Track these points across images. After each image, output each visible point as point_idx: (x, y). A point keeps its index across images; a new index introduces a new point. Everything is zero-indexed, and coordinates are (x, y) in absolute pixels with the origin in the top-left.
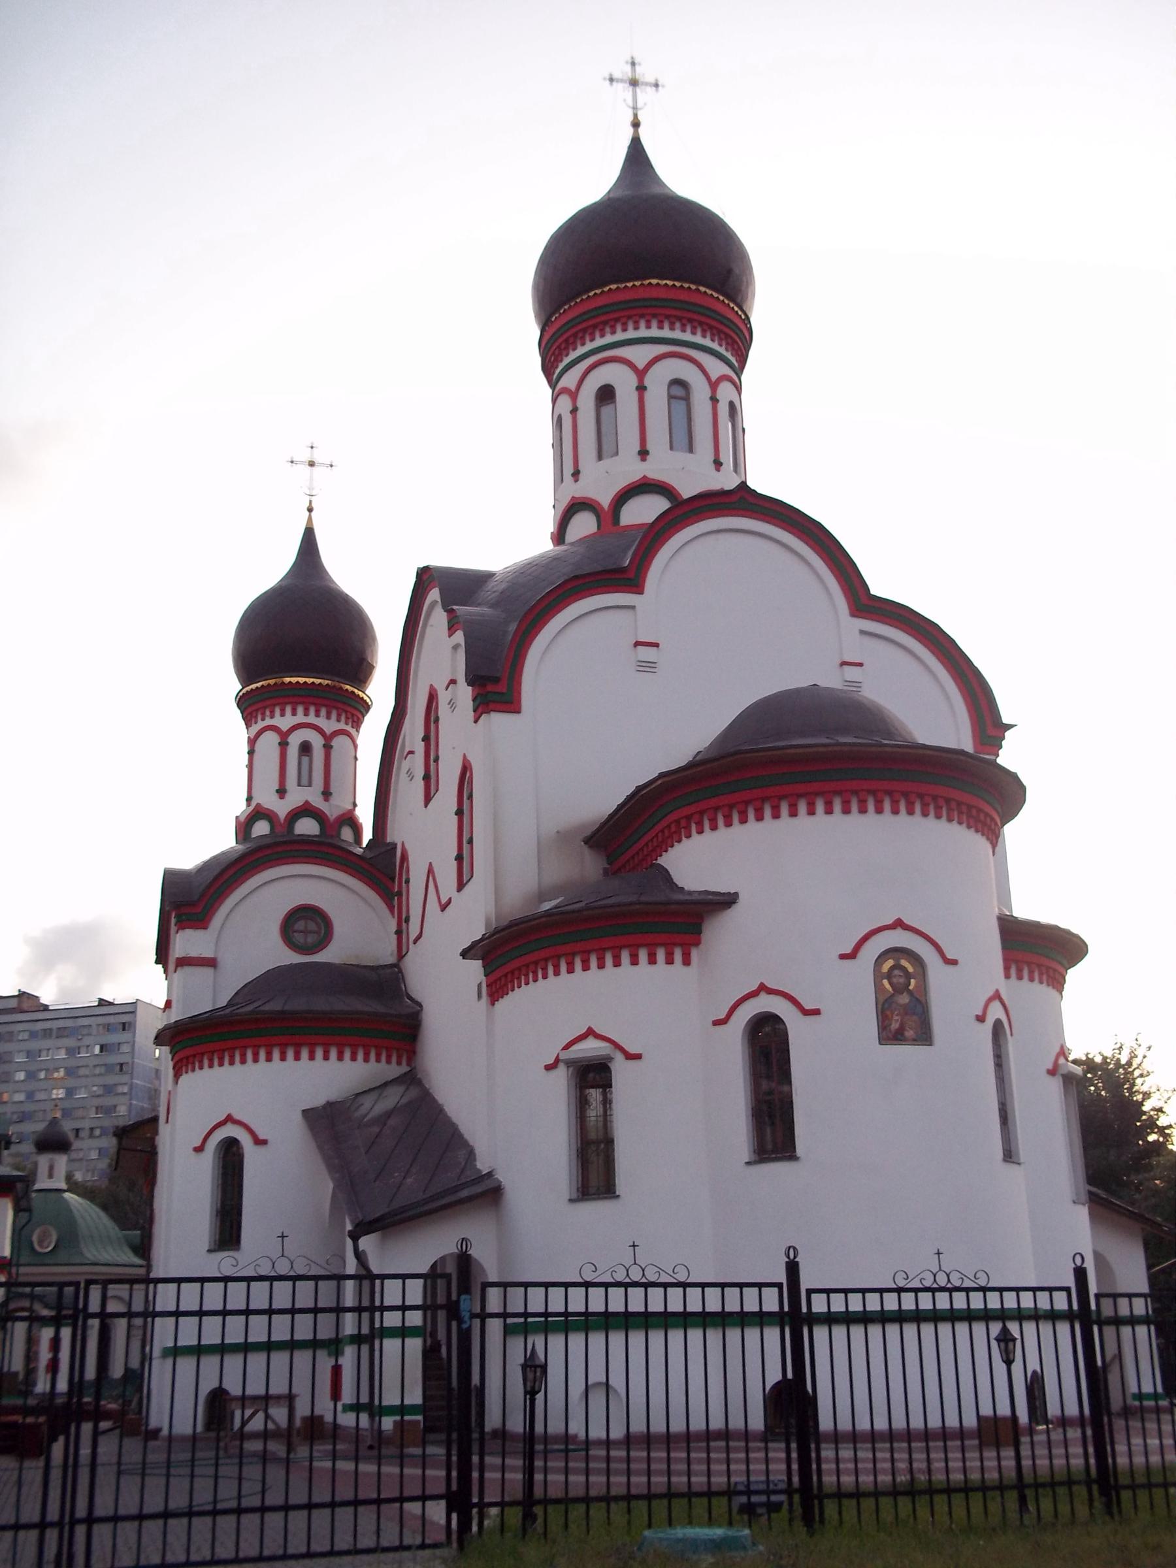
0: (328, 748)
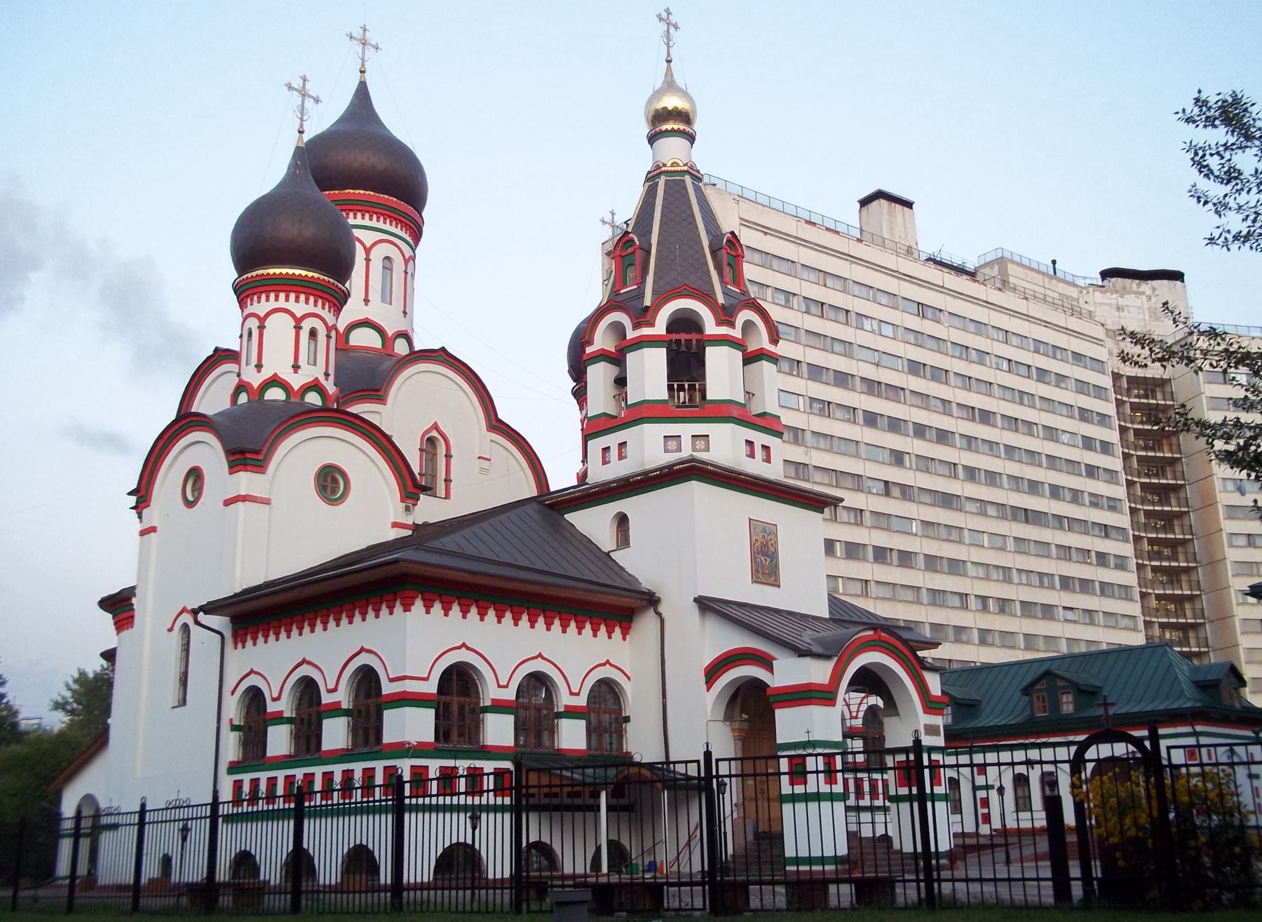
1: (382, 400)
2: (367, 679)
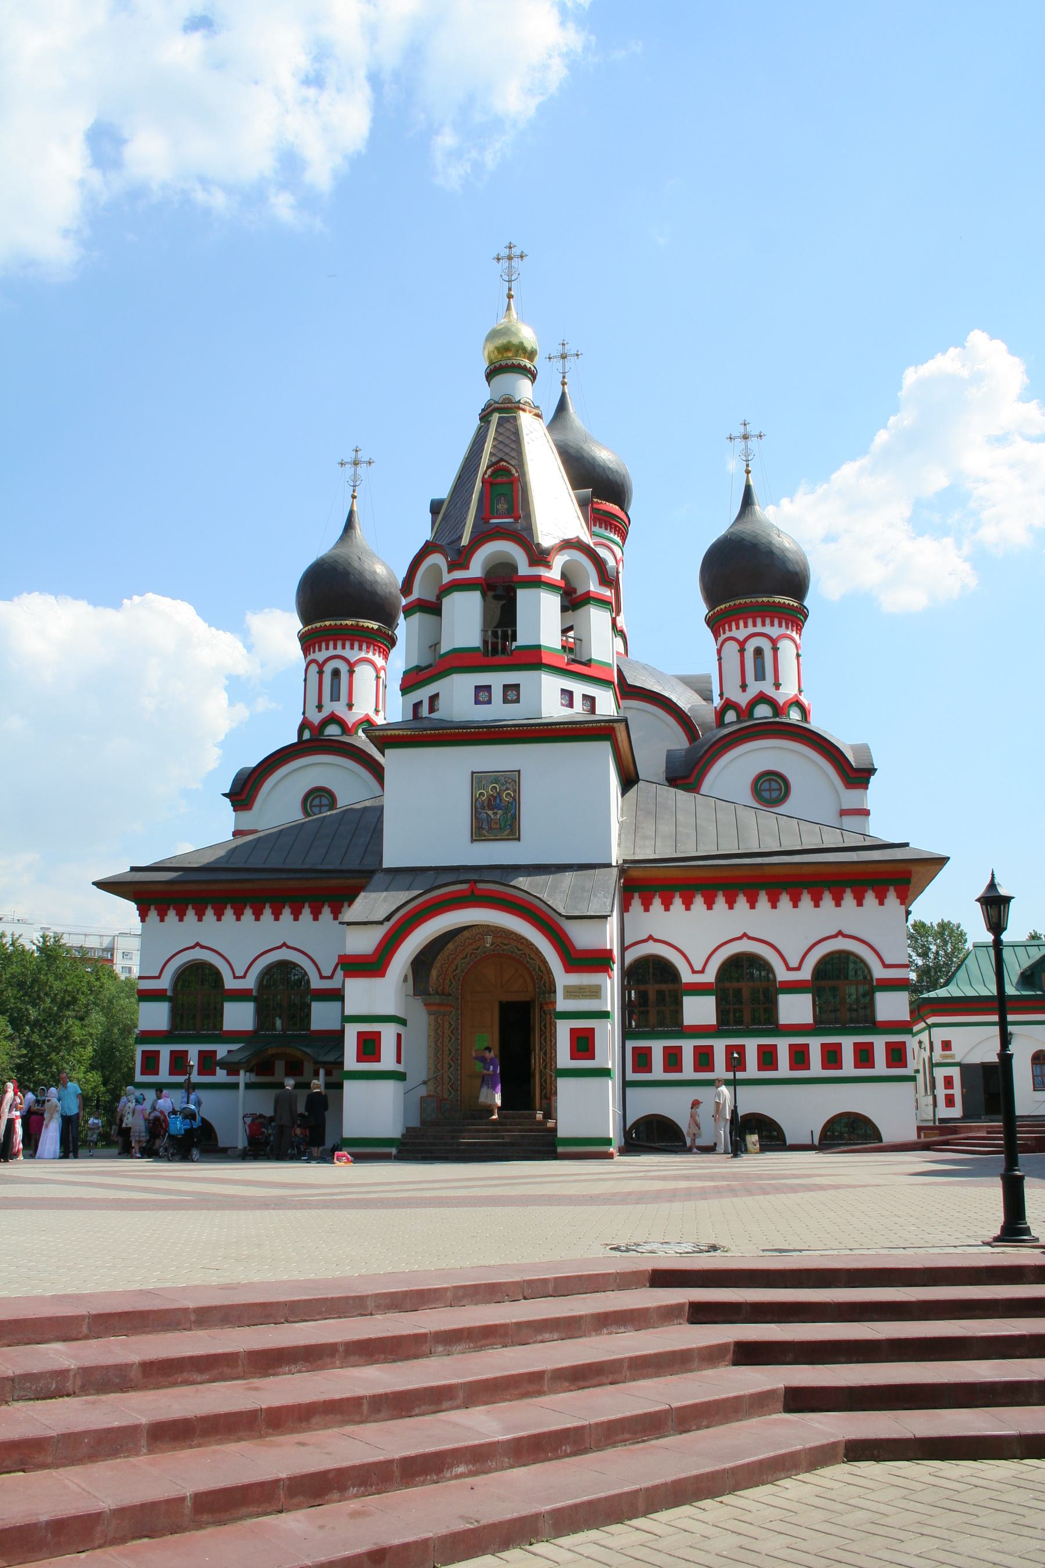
0: (775, 650)
1: (367, 715)
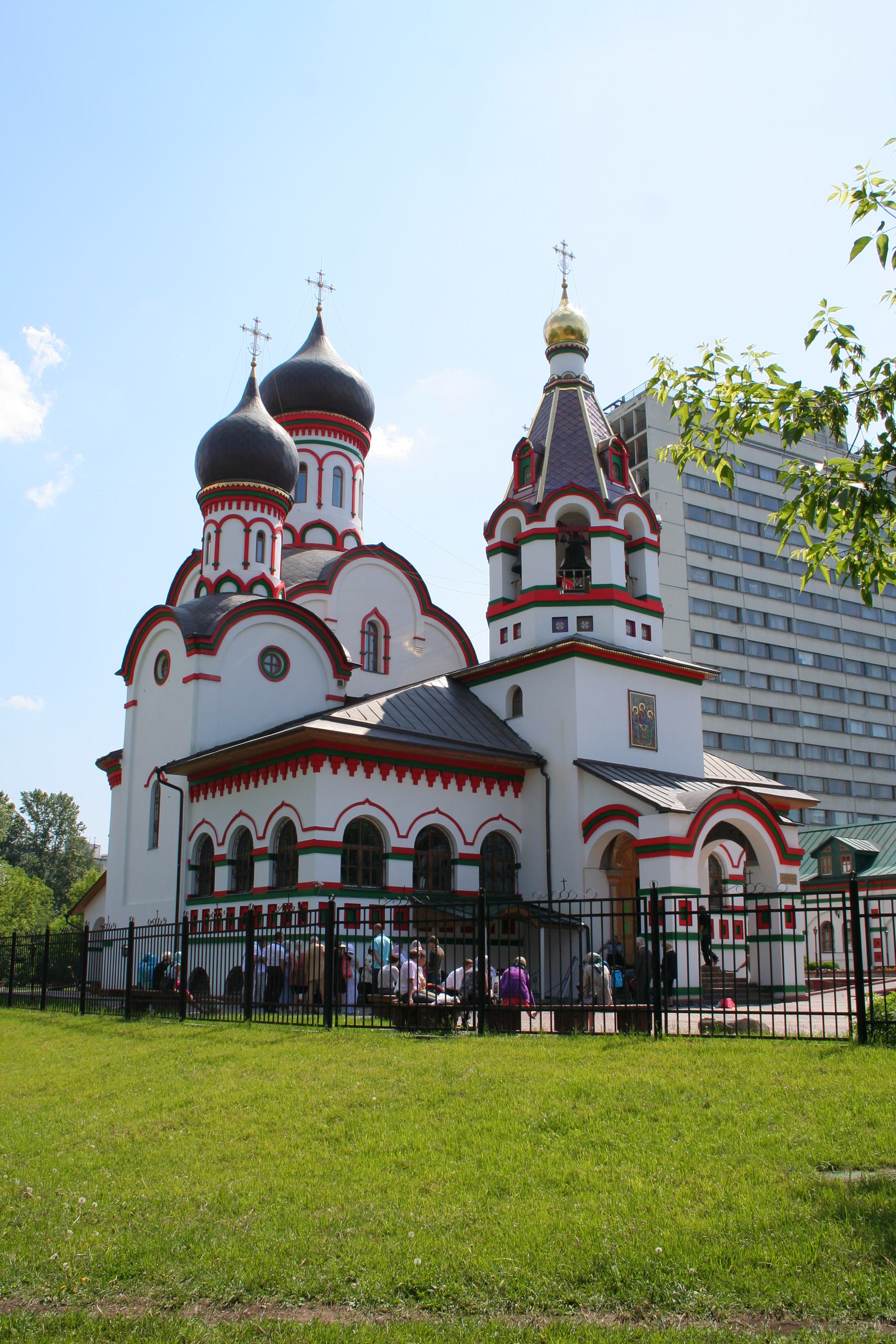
2: (287, 830)
